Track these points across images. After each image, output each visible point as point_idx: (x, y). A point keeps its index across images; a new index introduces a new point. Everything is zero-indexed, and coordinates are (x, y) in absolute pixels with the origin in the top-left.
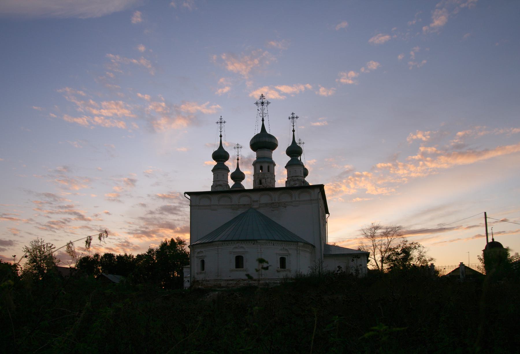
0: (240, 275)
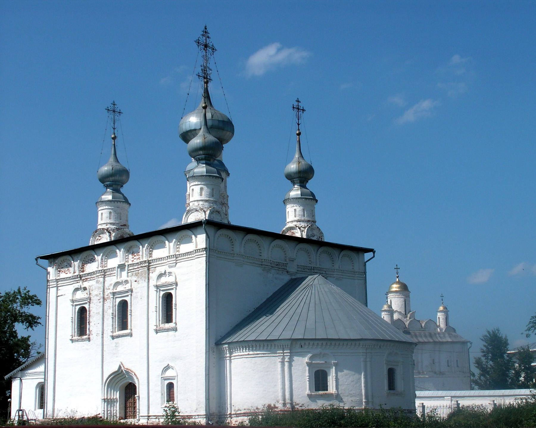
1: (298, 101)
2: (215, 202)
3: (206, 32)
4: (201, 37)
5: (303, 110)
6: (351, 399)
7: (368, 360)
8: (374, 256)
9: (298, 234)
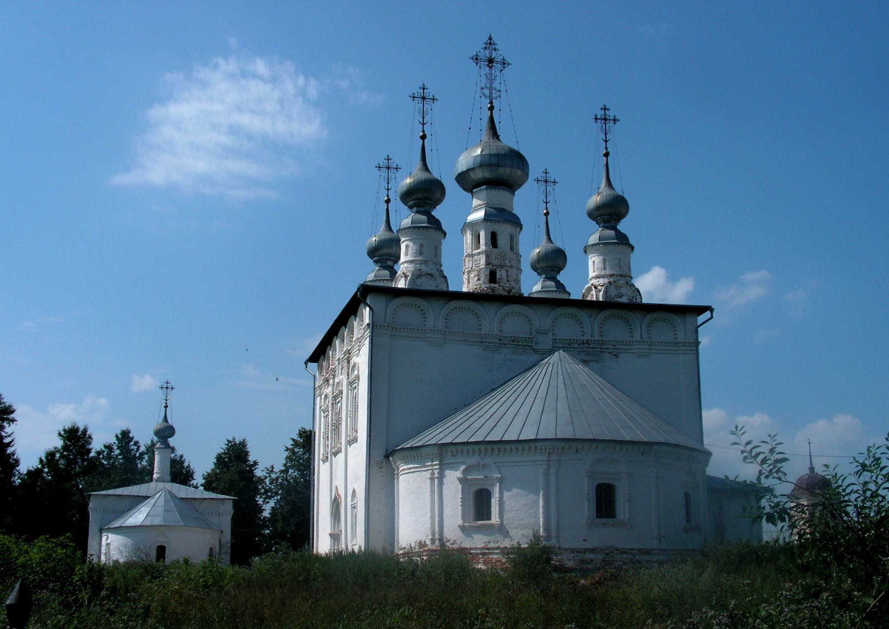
0: (607, 536)
1: (605, 109)
2: (425, 262)
3: (490, 44)
4: (482, 51)
5: (615, 120)
6: (521, 532)
7: (552, 471)
8: (712, 317)
9: (593, 296)
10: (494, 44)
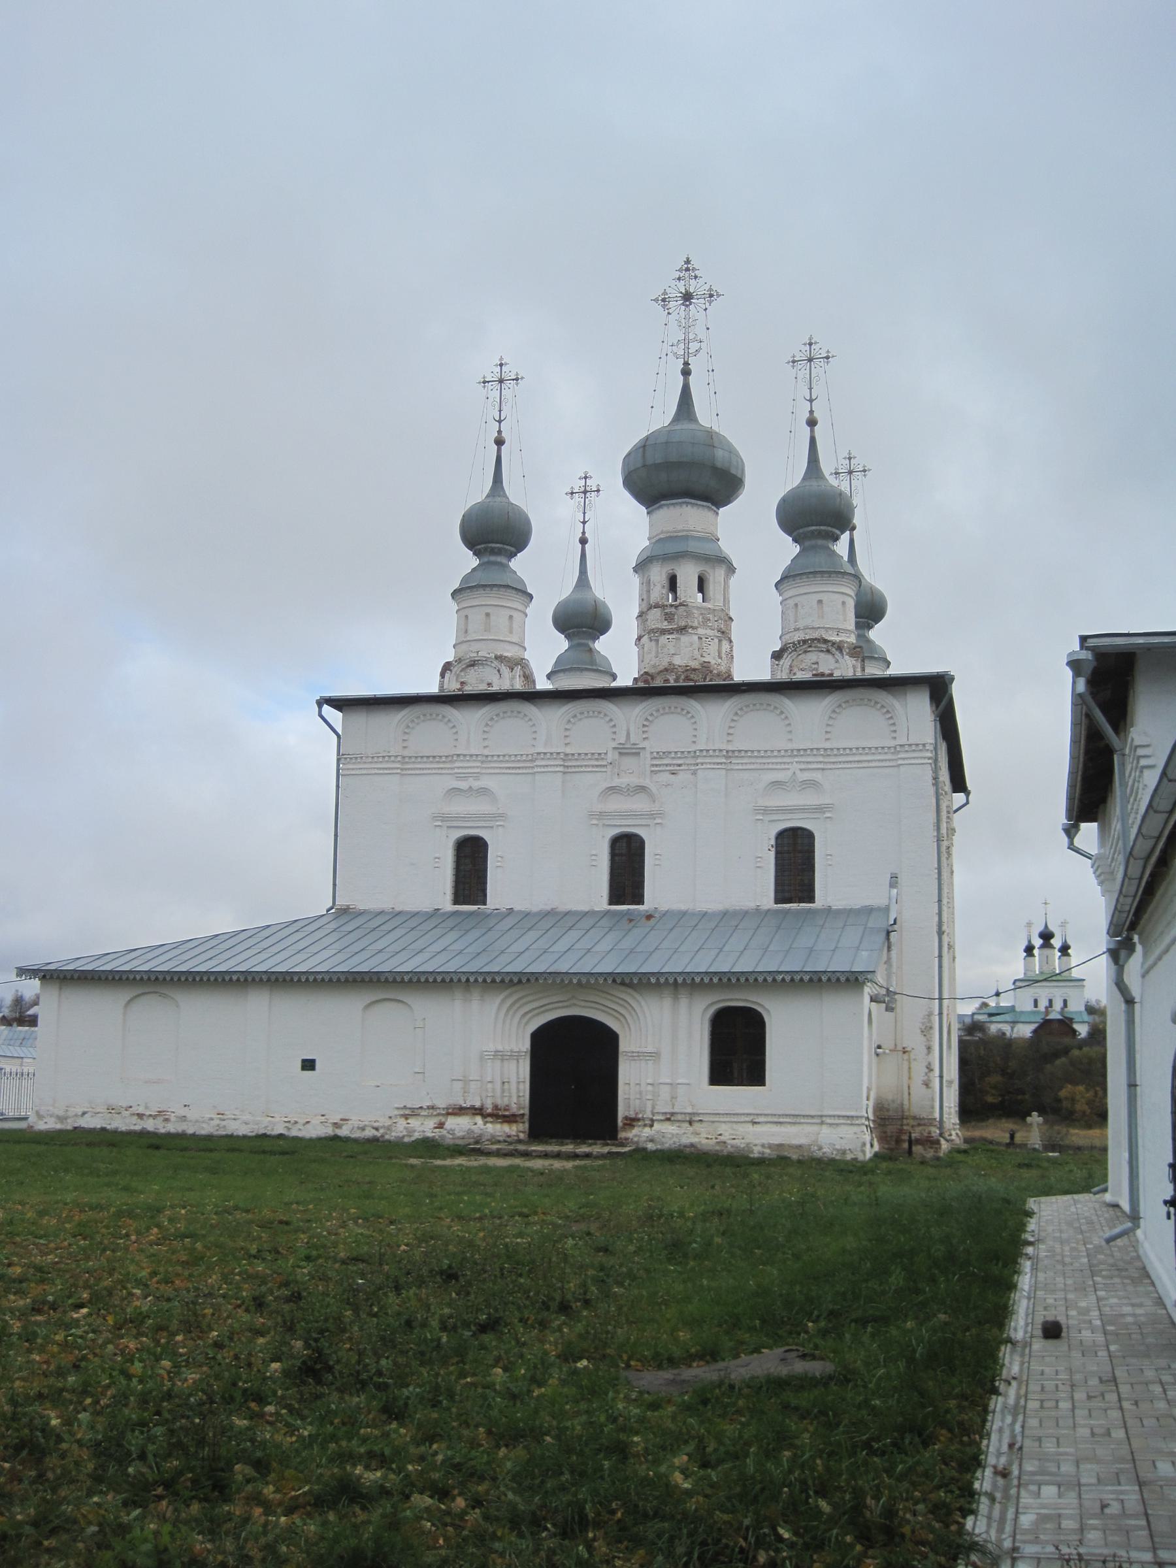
10: (694, 269)
